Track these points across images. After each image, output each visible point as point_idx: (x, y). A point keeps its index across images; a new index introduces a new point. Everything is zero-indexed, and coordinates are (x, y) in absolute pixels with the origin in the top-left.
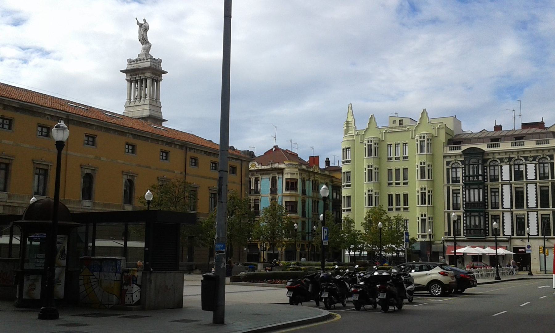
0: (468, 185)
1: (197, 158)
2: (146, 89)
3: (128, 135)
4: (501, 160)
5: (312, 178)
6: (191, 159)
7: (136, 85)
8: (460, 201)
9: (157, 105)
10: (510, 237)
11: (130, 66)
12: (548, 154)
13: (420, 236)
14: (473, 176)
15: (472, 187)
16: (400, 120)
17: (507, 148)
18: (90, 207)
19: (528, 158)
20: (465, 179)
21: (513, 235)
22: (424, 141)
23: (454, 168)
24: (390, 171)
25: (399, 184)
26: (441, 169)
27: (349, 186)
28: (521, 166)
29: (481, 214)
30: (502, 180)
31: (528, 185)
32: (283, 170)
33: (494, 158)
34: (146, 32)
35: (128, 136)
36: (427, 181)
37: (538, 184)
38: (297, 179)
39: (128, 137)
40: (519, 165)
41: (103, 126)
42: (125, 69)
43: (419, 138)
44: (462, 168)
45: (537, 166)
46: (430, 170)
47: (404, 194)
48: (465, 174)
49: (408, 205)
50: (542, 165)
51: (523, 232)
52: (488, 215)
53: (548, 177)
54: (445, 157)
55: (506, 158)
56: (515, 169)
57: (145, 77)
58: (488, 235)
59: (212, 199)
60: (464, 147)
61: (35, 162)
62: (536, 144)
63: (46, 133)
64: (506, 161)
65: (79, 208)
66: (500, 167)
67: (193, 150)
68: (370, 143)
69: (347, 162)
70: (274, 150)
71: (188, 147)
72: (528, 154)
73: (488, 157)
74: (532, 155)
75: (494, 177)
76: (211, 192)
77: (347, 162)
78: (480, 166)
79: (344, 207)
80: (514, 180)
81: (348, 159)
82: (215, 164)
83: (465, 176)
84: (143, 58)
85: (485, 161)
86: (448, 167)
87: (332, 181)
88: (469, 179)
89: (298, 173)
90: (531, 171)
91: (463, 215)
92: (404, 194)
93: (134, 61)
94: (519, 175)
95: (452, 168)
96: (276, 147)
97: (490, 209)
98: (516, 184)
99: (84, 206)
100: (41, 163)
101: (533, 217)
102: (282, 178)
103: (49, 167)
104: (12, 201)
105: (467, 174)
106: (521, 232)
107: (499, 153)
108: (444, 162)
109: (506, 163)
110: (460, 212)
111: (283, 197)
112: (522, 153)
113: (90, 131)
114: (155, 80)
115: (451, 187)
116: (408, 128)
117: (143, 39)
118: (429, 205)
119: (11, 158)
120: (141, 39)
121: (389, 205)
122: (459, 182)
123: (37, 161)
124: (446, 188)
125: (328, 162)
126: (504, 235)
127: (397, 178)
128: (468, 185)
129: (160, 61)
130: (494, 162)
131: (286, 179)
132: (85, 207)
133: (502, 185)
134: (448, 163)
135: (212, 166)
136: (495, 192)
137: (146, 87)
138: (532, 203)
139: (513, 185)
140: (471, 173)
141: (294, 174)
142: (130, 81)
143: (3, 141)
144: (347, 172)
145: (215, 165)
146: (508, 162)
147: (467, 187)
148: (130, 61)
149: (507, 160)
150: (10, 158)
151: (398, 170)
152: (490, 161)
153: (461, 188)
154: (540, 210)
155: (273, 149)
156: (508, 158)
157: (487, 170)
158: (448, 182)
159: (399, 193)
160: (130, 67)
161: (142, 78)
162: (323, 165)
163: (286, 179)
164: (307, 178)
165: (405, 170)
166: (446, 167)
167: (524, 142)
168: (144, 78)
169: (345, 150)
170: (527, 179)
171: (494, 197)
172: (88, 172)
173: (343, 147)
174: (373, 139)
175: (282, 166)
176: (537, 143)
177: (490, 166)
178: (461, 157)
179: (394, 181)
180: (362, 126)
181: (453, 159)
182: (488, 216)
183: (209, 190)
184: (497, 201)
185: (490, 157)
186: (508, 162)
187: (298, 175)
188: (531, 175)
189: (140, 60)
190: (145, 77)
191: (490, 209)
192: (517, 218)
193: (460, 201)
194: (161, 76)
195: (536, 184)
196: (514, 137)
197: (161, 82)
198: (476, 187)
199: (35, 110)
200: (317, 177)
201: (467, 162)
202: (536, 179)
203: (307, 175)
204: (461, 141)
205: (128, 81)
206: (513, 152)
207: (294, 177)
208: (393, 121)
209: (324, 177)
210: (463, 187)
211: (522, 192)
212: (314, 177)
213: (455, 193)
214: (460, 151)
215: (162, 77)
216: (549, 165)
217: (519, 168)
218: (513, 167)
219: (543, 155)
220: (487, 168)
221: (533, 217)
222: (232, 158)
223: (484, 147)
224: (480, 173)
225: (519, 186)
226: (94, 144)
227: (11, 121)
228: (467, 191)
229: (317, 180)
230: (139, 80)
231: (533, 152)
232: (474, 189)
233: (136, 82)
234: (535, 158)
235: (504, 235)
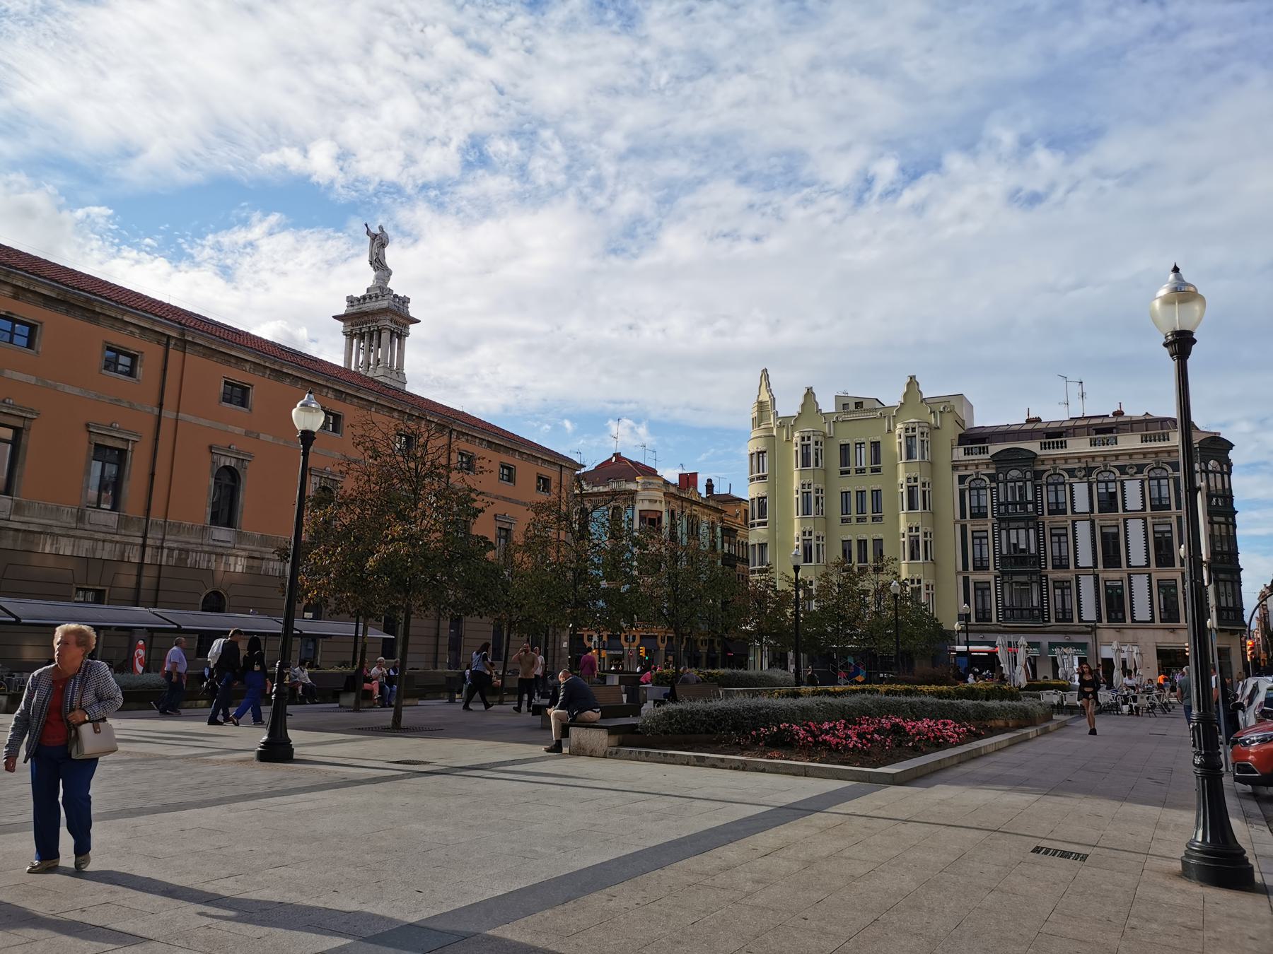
0: (1005, 521)
1: (473, 453)
2: (380, 349)
3: (325, 390)
4: (1071, 472)
5: (688, 511)
6: (460, 456)
7: (362, 344)
8: (989, 552)
9: (398, 379)
10: (1093, 624)
11: (352, 308)
12: (1169, 460)
15: (1012, 525)
16: (856, 403)
17: (1084, 449)
18: (229, 542)
19: (1127, 469)
20: (998, 510)
21: (1100, 620)
23: (974, 489)
24: (846, 494)
26: (950, 487)
27: (765, 524)
28: (1110, 485)
30: (1073, 512)
31: (1129, 521)
32: (634, 493)
33: (1055, 469)
34: (383, 247)
35: (325, 394)
36: (922, 513)
37: (1149, 519)
38: (661, 512)
39: (326, 396)
40: (1106, 482)
41: (267, 364)
42: (343, 312)
43: (903, 430)
44: (991, 489)
45: (1146, 483)
46: (927, 493)
48: (998, 499)
50: (1155, 482)
51: (1120, 615)
52: (1047, 579)
53: (986, 513)
54: (955, 468)
55: (1080, 469)
56: (1100, 491)
57: (378, 327)
58: (1046, 621)
59: (502, 540)
60: (994, 449)
61: (91, 430)
62: (1142, 442)
63: (128, 369)
64: (1079, 474)
65: (202, 544)
66: (1068, 486)
67: (466, 437)
68: (806, 442)
69: (758, 478)
70: (614, 460)
71: (454, 430)
72: (1126, 460)
73: (1042, 468)
74: (1134, 462)
76: (499, 524)
77: (758, 478)
78: (1029, 484)
79: (754, 565)
80: (1099, 513)
81: (761, 474)
82: (509, 469)
83: (999, 504)
84: (376, 294)
85: (1038, 475)
86: (962, 487)
87: (722, 520)
88: (1007, 510)
89: (663, 500)
90: (1133, 493)
92: (859, 541)
93: (358, 300)
94: (1109, 502)
95: (971, 489)
96: (617, 455)
97: (1050, 567)
98: (1106, 520)
99: (214, 540)
100: (108, 434)
101: (1140, 583)
102: (633, 509)
103: (130, 445)
104: (22, 519)
105: (1002, 500)
106: (1116, 616)
107: (1066, 460)
108: (954, 477)
109: (1080, 479)
112: (1114, 458)
113: (237, 375)
114: (397, 333)
115: (969, 526)
117: (377, 260)
118: (926, 561)
119: (29, 416)
120: (373, 262)
122: (985, 515)
123: (99, 428)
124: (958, 527)
125: (710, 486)
126: (1080, 620)
127: (861, 510)
128: (1005, 521)
129: (405, 301)
130: (1055, 477)
131: (640, 511)
132: (216, 543)
133: (1125, 520)
134: (962, 479)
135: (503, 474)
137: (379, 347)
138: (1138, 558)
139: (1097, 522)
141: (656, 501)
142: (350, 336)
143: (8, 373)
144: (759, 498)
145: (509, 472)
147: (1003, 525)
148: (351, 300)
149: (1083, 473)
150: (24, 415)
151: (861, 494)
152: (1045, 475)
155: (611, 459)
156: (1084, 468)
157: (1042, 491)
159: (864, 537)
160: (354, 310)
161: (372, 329)
162: (702, 489)
163: (640, 511)
164: (678, 511)
165: (877, 493)
166: (957, 487)
167: (1116, 438)
168: (376, 329)
169: (755, 456)
170: (1125, 510)
171: (1057, 544)
172: (228, 464)
173: (752, 451)
174: (812, 433)
175: (632, 486)
176: (1145, 439)
177: (1048, 484)
180: (789, 406)
181: (971, 471)
182: (1047, 582)
183: (496, 520)
184: (1064, 553)
185: (1048, 467)
186: (1084, 476)
187: (663, 503)
188: (1134, 502)
189: (370, 297)
190: (378, 327)
191: (1050, 567)
192: (1107, 587)
193: (989, 552)
194: (406, 327)
195: (1145, 520)
196: (1094, 429)
197: (407, 338)
198: (1022, 524)
199: (98, 310)
200: (696, 511)
202: (1144, 509)
203: (678, 506)
204: (986, 438)
205: (346, 335)
206: (1093, 458)
207: (657, 507)
208: (844, 405)
209: (709, 512)
211: (1116, 535)
212: (691, 511)
213: (977, 538)
214: (988, 456)
215: (409, 328)
216: (1171, 482)
217: (1107, 488)
218: (1094, 486)
219: (1159, 462)
220: (1041, 489)
221: (1140, 583)
222: (542, 459)
223: (1034, 446)
224: (1030, 498)
225: (1109, 523)
226: (244, 403)
227: (33, 328)
228: (1004, 533)
229: (696, 516)
230: (367, 332)
231: (1135, 456)
232: (1017, 529)
233: (362, 337)
234: (1140, 469)
235: (1080, 620)
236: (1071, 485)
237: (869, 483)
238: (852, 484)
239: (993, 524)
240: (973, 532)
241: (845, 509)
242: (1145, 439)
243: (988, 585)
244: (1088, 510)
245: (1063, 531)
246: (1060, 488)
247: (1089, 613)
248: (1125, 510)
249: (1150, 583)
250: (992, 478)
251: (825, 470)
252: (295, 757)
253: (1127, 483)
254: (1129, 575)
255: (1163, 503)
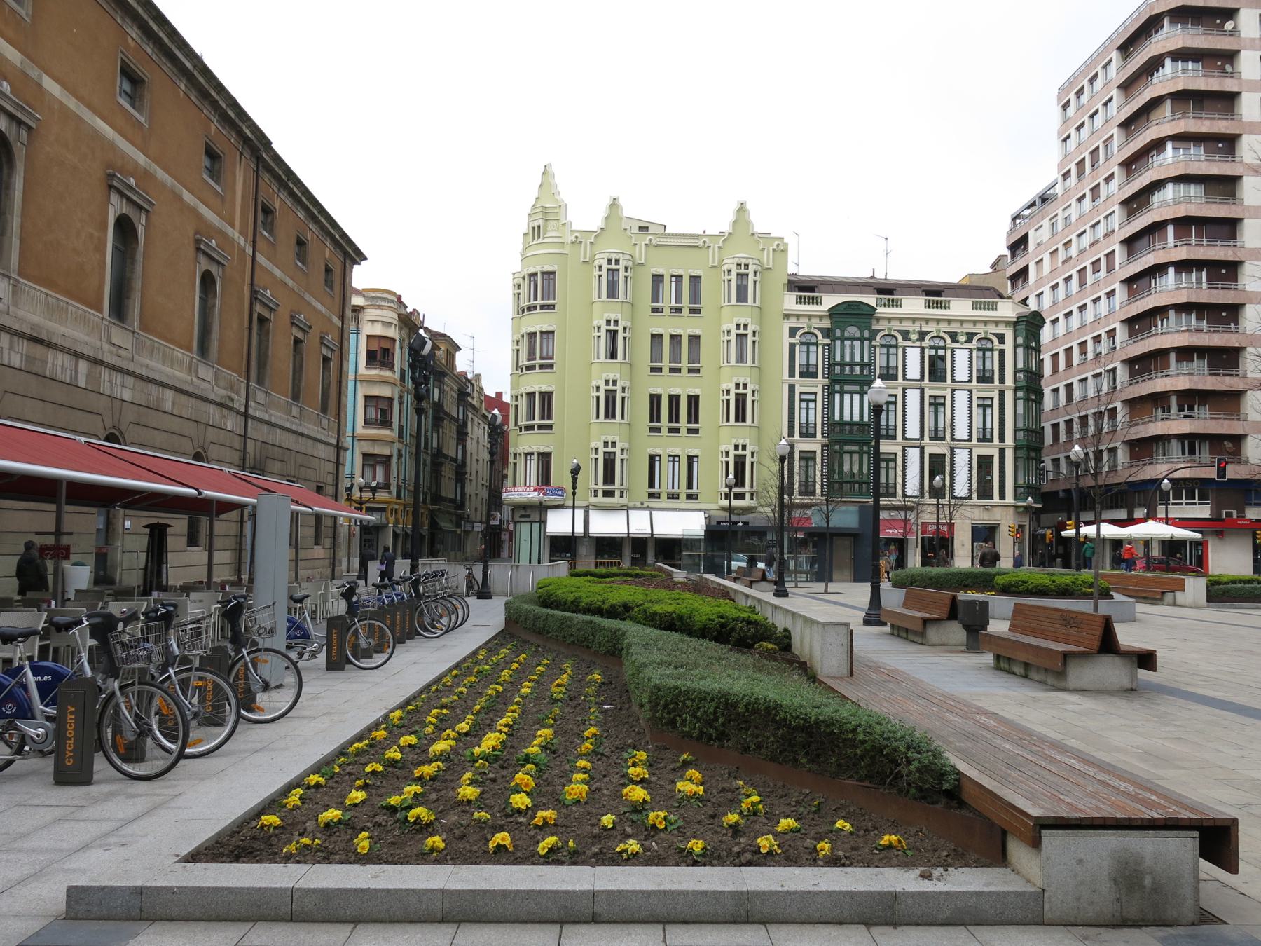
13: (600, 493)
14: (862, 365)
15: (847, 388)
22: (747, 275)
25: (678, 370)
29: (865, 448)
30: (905, 379)
47: (689, 396)
49: (549, 418)
53: (816, 373)
66: (900, 351)
75: (808, 369)
81: (532, 302)
86: (793, 340)
91: (822, 450)
92: (690, 397)
110: (897, 445)
111: (358, 383)
115: (797, 387)
116: (704, 242)
121: (651, 421)
127: (675, 357)
133: (904, 389)
134: (793, 332)
136: (808, 401)
140: (857, 359)
146: (918, 340)
151: (675, 338)
152: (880, 335)
153: (819, 390)
154: (929, 445)
158: (792, 374)
166: (787, 341)
176: (976, 307)
178: (821, 320)
179: (666, 363)
181: (803, 323)
195: (970, 391)
201: (838, 333)
206: (927, 321)
210: (823, 389)
223: (870, 300)
228: (837, 396)
232: (852, 393)
234: (970, 337)
235: (904, 496)
236: (904, 349)
237: (685, 326)
238: (667, 326)
239: (823, 386)
240: (801, 393)
241: (656, 355)
242: (976, 307)
243: (812, 455)
244: (918, 377)
245: (812, 397)
246: (988, 354)
247: (961, 489)
248: (953, 380)
249: (971, 458)
250: (828, 333)
251: (632, 304)
252: (1196, 834)
253: (957, 352)
254: (904, 448)
255: (811, 370)
